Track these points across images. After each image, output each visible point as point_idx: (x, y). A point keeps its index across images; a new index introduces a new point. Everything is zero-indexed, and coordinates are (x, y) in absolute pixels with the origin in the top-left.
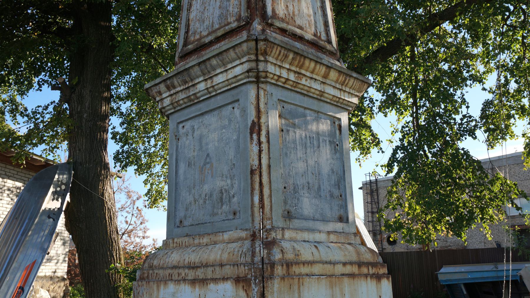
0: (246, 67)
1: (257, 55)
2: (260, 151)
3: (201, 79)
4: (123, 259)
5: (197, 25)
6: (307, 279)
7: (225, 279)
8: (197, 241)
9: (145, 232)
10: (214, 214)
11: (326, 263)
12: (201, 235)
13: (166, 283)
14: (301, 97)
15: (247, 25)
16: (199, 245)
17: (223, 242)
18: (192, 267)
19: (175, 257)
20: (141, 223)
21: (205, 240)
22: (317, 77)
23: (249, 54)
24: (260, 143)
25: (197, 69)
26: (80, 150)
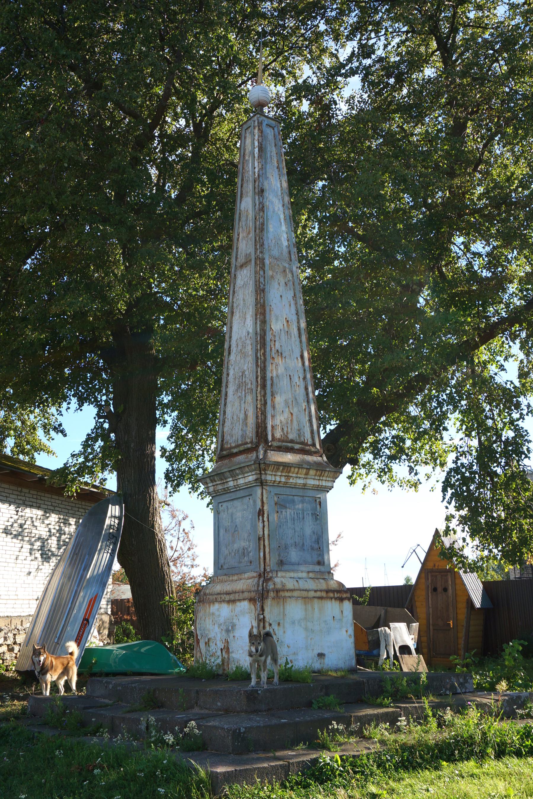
0: (255, 477)
1: (260, 471)
2: (264, 526)
3: (231, 479)
4: (175, 592)
5: (229, 437)
6: (289, 600)
7: (244, 599)
8: (231, 578)
9: (194, 560)
10: (240, 562)
11: (303, 590)
12: (233, 575)
13: (213, 603)
14: (291, 489)
15: (255, 449)
16: (232, 581)
17: (244, 579)
18: (228, 593)
19: (218, 588)
20: (189, 549)
21: (235, 578)
22: (301, 476)
23: (255, 470)
24: (263, 521)
25: (228, 474)
26: (128, 481)
